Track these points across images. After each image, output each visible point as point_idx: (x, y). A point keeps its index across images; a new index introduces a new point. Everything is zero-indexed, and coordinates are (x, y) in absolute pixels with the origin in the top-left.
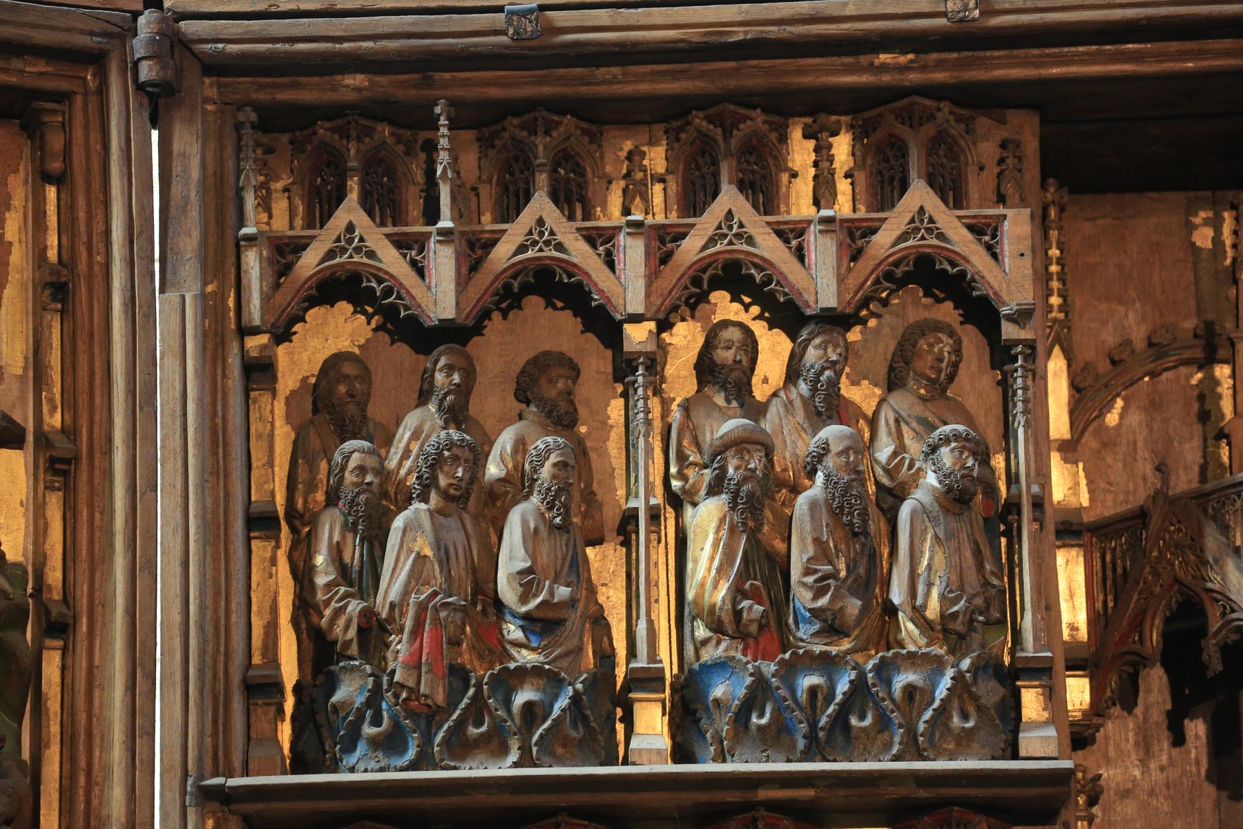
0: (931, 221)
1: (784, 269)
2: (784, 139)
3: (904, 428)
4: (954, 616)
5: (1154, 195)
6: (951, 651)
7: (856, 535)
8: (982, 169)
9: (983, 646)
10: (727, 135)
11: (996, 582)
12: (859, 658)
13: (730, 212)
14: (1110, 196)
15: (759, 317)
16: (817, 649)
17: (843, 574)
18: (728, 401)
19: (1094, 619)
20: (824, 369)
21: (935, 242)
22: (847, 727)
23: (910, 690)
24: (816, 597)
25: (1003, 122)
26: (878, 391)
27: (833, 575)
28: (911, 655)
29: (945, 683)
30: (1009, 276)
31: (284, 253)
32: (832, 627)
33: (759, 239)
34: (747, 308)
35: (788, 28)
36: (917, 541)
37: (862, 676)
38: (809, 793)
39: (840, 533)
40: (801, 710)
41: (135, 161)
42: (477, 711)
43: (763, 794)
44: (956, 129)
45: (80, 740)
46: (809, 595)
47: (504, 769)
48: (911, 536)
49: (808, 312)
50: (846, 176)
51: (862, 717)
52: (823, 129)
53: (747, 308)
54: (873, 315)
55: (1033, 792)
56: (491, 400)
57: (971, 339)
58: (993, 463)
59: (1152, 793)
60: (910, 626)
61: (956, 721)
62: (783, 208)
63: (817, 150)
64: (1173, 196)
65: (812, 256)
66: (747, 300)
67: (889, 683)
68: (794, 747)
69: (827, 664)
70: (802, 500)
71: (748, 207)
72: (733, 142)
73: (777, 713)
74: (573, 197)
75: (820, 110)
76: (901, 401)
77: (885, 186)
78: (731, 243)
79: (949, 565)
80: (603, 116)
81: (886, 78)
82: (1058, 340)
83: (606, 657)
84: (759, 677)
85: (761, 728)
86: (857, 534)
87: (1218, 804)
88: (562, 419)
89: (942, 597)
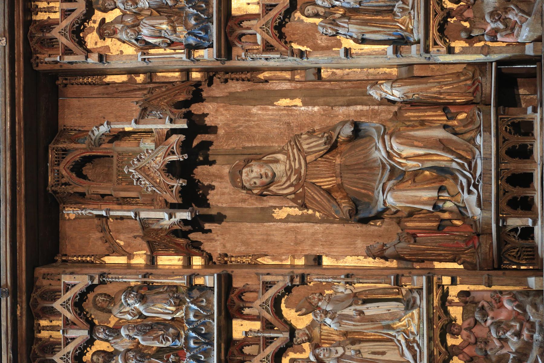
0: (64, 302)
1: (77, 344)
2: (40, 339)
3: (122, 311)
4: (175, 303)
5: (60, 229)
6: (185, 304)
7: (152, 328)
8: (50, 284)
9: (183, 293)
10: (39, 357)
11: (166, 288)
12: (186, 329)
13: (61, 305)
14: (60, 240)
15: (90, 348)
16: (183, 341)
17: (163, 332)
18: (114, 360)
19: (177, 254)
20: (105, 333)
21: (70, 301)
22: (205, 334)
23: (195, 316)
24: (169, 341)
25: (38, 278)
26: (112, 316)
27: (163, 335)
28: (185, 315)
29: (193, 306)
32: (177, 336)
33: (68, 351)
34: (88, 351)
35: (9, 341)
36: (154, 312)
37: (191, 329)
38: (223, 345)
39: (151, 332)
40: (200, 346)
43: (223, 358)
44: (39, 292)
46: (168, 342)
48: (152, 313)
49: (89, 337)
50: (49, 4)
51: (202, 330)
52: (38, 329)
53: (88, 351)
54: (91, 316)
55: (223, 284)
57: (98, 290)
58: (133, 285)
59: (224, 239)
60: (177, 314)
61: (204, 304)
62: (60, 340)
63: (43, 330)
64: (60, 224)
65: (73, 336)
66: (85, 351)
67: (193, 321)
68: (210, 349)
69: (187, 338)
70: (142, 343)
71: (59, 300)
72: (41, 355)
73: (201, 353)
75: (33, 329)
76: (115, 311)
78: (268, 306)
79: (161, 303)
81: (24, 313)
82: (100, 259)
84: (190, 357)
85: (205, 358)
86: (152, 327)
87: (227, 222)
89: (170, 306)
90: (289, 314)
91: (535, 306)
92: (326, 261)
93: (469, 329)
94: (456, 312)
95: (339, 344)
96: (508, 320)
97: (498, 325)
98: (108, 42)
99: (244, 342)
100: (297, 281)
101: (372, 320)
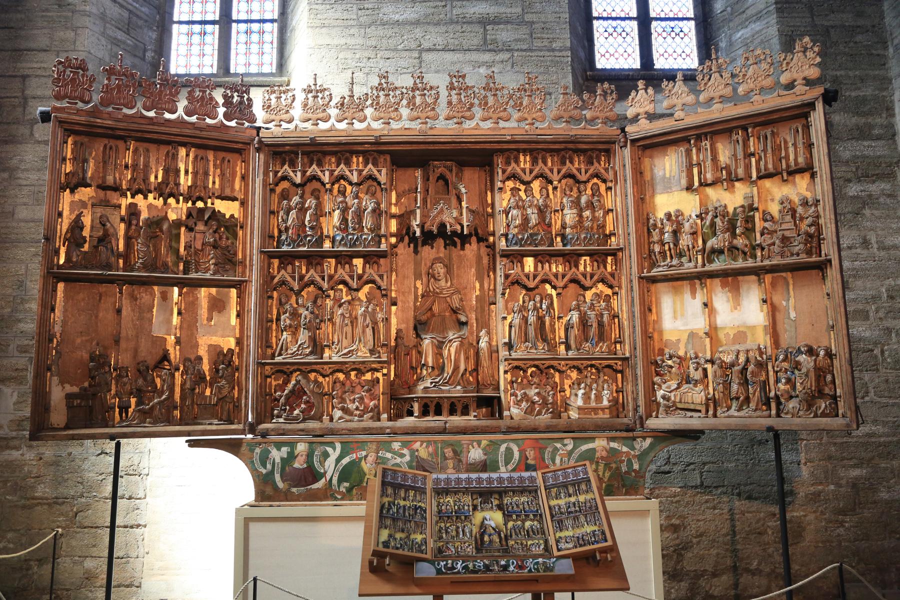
30: (383, 178)
31: (276, 173)
41: (254, 158)
42: (301, 241)
45: (244, 243)
47: (305, 249)
56: (307, 195)
57: (378, 188)
74: (320, 164)
77: (366, 164)
80: (325, 154)
83: (322, 233)
88: (317, 198)
90: (366, 288)
91: (372, 418)
92: (394, 308)
93: (359, 383)
94: (368, 376)
95: (351, 315)
96: (364, 403)
97: (362, 398)
98: (509, 193)
99: (351, 265)
100: (384, 292)
101: (364, 332)
